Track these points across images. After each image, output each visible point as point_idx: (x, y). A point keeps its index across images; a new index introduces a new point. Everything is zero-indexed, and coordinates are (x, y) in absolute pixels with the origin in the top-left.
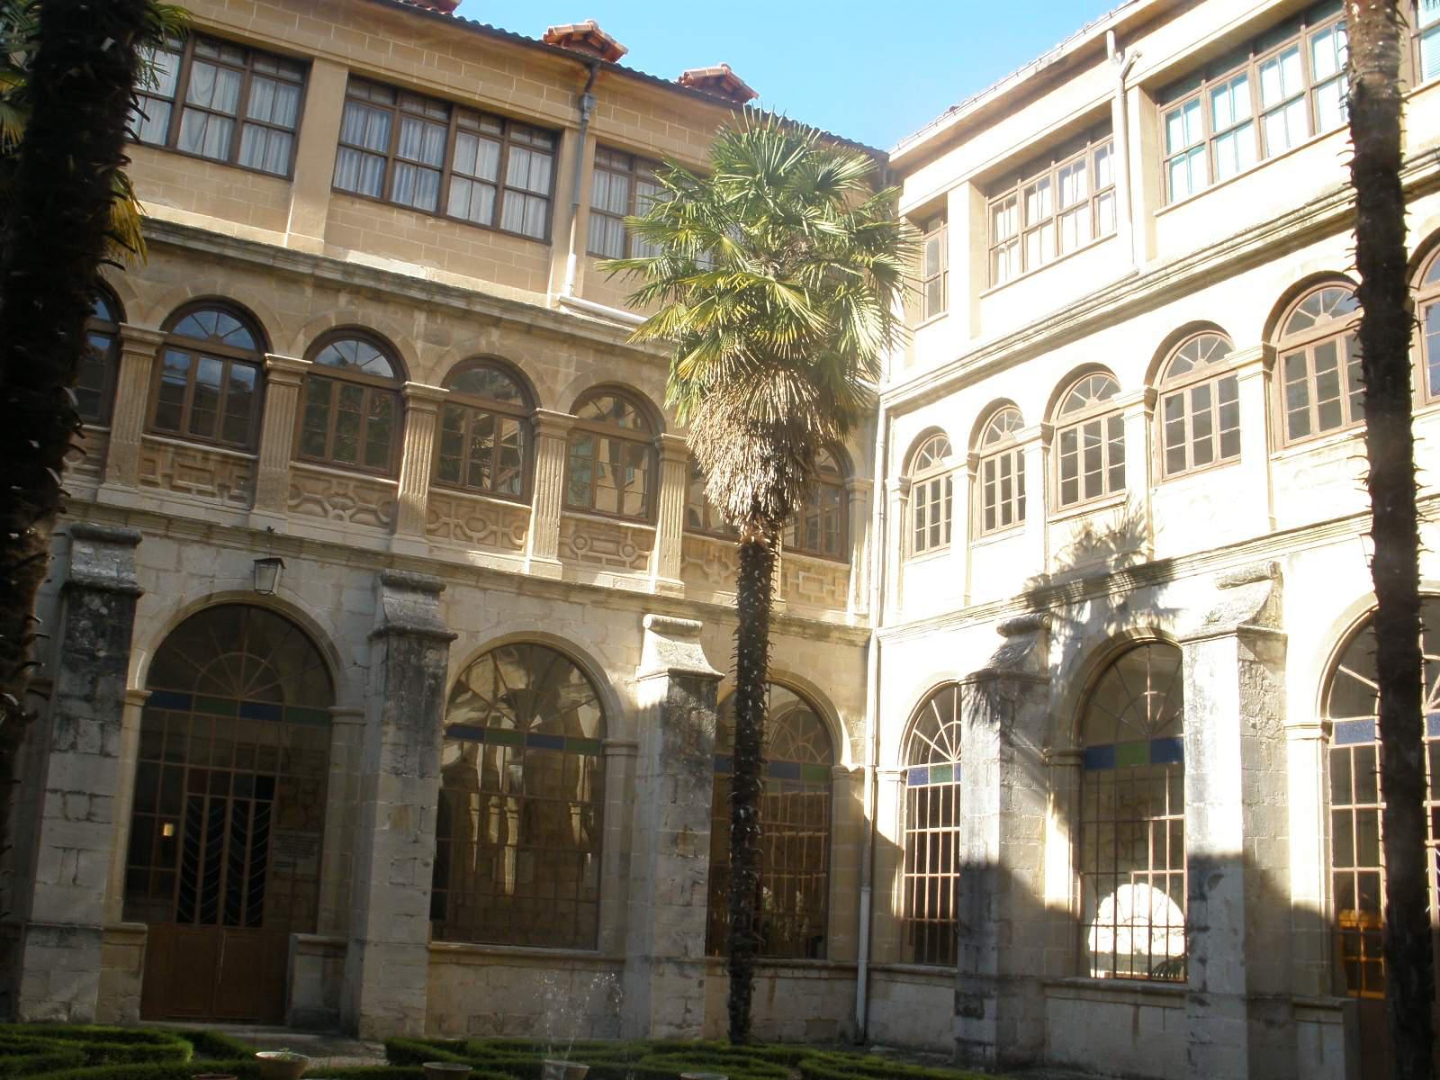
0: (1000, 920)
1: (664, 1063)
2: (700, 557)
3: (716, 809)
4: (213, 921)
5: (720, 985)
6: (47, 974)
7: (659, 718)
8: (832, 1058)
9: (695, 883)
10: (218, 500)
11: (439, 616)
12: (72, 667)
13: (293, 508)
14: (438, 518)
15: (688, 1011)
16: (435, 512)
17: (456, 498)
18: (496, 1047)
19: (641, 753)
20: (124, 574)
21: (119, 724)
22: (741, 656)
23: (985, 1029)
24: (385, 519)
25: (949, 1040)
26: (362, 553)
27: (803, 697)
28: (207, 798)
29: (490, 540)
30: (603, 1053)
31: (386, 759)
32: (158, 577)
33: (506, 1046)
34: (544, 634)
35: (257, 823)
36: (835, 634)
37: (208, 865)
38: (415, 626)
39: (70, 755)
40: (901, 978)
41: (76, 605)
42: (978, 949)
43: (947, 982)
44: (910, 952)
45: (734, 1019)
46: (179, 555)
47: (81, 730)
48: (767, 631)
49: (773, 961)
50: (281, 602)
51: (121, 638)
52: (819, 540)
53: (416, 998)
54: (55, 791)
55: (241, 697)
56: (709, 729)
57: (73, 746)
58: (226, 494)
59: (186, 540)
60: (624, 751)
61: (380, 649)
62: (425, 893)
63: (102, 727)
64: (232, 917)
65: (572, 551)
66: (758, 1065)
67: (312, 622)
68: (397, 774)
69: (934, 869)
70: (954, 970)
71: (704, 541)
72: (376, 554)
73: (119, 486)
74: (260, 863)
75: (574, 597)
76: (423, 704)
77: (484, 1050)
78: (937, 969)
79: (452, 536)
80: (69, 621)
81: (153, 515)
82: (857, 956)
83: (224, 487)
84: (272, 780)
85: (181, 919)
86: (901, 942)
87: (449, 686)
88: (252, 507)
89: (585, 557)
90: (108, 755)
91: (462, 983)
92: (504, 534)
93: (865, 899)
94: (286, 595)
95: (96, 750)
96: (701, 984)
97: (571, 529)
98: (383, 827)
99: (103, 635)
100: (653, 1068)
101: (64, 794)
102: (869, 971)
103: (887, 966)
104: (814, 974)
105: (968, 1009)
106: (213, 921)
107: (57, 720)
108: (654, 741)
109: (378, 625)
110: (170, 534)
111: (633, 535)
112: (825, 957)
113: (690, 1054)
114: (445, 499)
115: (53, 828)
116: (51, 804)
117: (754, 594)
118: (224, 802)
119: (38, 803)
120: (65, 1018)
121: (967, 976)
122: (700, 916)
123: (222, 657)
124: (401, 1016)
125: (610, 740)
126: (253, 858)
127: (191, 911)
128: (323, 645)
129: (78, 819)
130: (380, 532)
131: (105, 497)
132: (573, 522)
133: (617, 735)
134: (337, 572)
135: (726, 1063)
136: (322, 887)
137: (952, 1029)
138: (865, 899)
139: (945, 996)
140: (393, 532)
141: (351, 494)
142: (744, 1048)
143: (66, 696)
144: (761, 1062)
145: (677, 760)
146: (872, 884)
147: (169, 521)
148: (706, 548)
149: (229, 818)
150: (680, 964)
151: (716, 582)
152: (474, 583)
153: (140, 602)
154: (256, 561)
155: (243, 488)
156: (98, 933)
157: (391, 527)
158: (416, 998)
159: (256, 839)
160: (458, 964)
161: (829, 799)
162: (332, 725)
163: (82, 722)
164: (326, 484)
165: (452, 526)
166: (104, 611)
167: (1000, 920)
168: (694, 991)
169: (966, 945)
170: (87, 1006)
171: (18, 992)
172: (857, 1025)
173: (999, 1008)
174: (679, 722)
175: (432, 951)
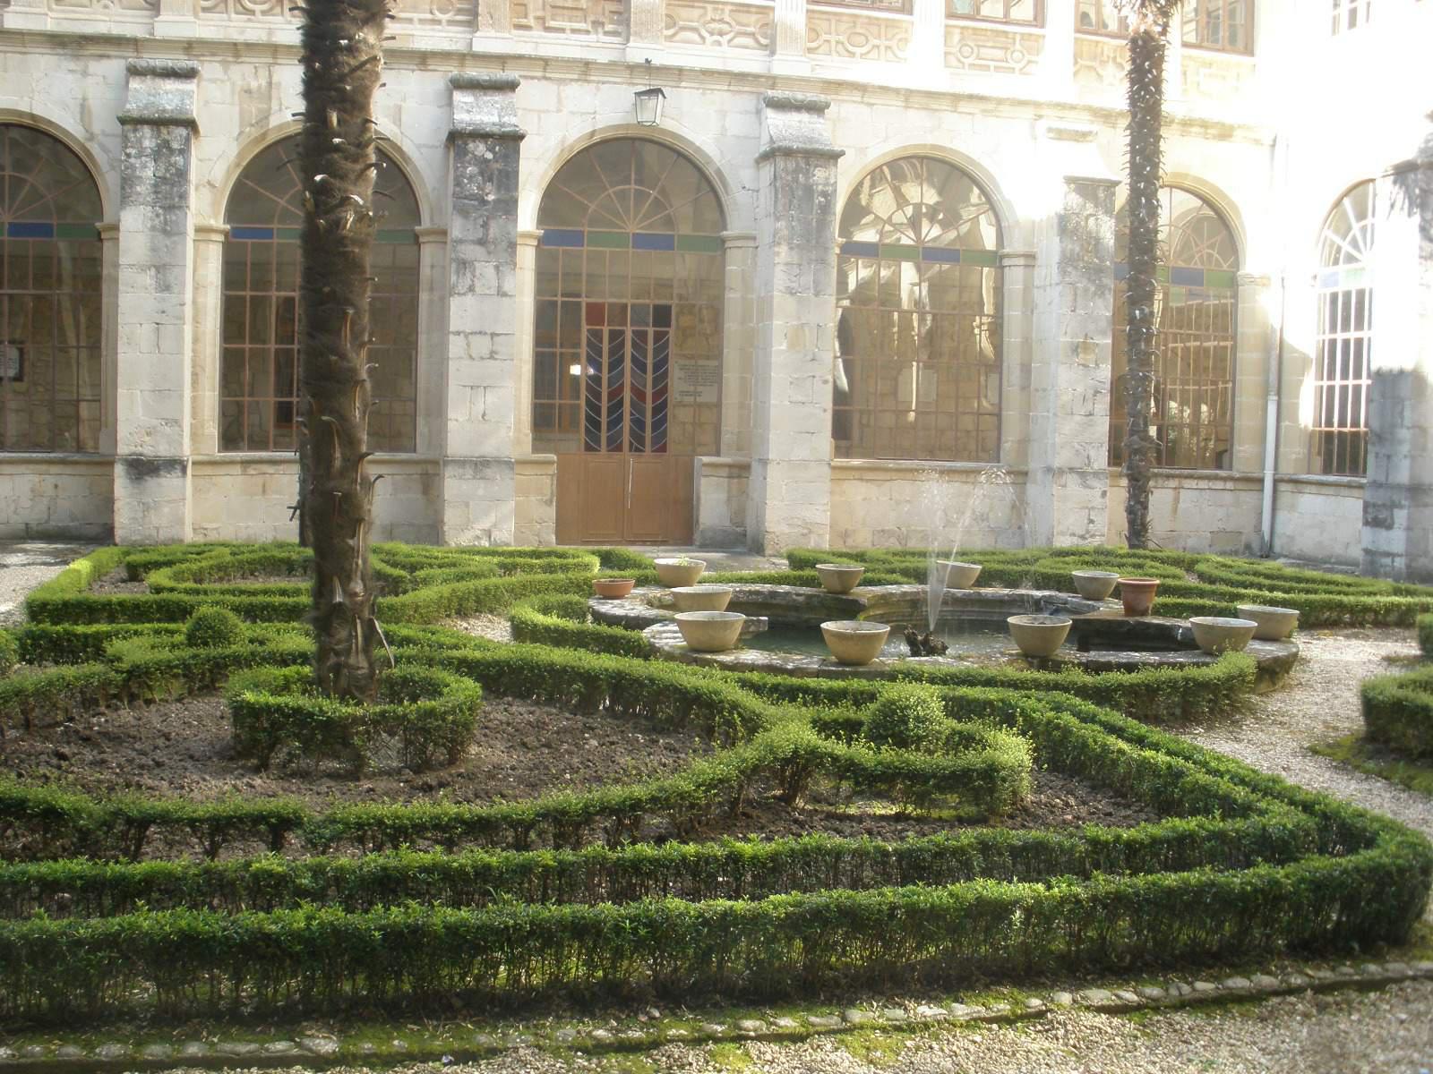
0: (1414, 427)
1: (1061, 565)
2: (1095, 58)
3: (1115, 318)
4: (619, 448)
5: (1119, 494)
6: (467, 505)
7: (1055, 226)
8: (1230, 563)
9: (1097, 392)
10: (593, 37)
11: (825, 134)
12: (464, 213)
13: (670, 38)
14: (818, 35)
15: (1091, 521)
16: (814, 30)
17: (835, 14)
18: (895, 554)
19: (1039, 262)
20: (505, 119)
21: (513, 264)
22: (1133, 152)
23: (1395, 540)
24: (764, 41)
25: (1356, 553)
26: (741, 77)
27: (1206, 201)
28: (606, 330)
29: (874, 54)
30: (1002, 558)
31: (780, 279)
32: (539, 118)
33: (904, 554)
34: (934, 147)
35: (657, 351)
36: (1237, 133)
37: (611, 395)
38: (801, 145)
39: (469, 298)
40: (1308, 489)
41: (461, 153)
42: (1389, 457)
43: (1356, 492)
44: (1318, 462)
45: (1132, 523)
46: (559, 94)
47: (477, 273)
48: (1160, 125)
49: (1178, 472)
50: (664, 131)
51: (507, 179)
52: (1221, 34)
53: (820, 514)
54: (458, 333)
55: (633, 228)
56: (1108, 237)
57: (471, 289)
58: (600, 30)
59: (564, 80)
60: (1022, 261)
61: (767, 171)
62: (825, 411)
63: (497, 268)
64: (638, 445)
65: (959, 61)
66: (1152, 567)
67: (698, 149)
68: (791, 294)
69: (1345, 376)
70: (1364, 481)
71: (1097, 42)
72: (757, 77)
73: (492, 33)
74: (661, 392)
75: (964, 107)
76: (814, 224)
77: (883, 557)
78: (1346, 479)
79: (834, 53)
80: (456, 169)
81: (530, 58)
82: (1262, 466)
83: (597, 24)
84: (669, 308)
85: (589, 448)
86: (1310, 452)
87: (839, 205)
88: (628, 40)
89: (972, 66)
90: (505, 295)
91: (864, 499)
92: (888, 48)
93: (1272, 408)
94: (668, 124)
95: (493, 291)
96: (1104, 494)
97: (956, 38)
98: (779, 346)
99: (490, 180)
100: (1050, 571)
101: (467, 335)
102: (1276, 482)
103: (1294, 477)
104: (1220, 485)
105: (1376, 519)
106: (619, 448)
107: (454, 265)
108: (1051, 249)
109: (765, 148)
110: (548, 75)
111: (1022, 39)
112: (1231, 468)
113: (1087, 558)
114: (825, 16)
115: (459, 371)
116: (455, 346)
117: (1144, 87)
118: (622, 333)
119: (442, 347)
120: (487, 544)
121: (1376, 485)
122: (1102, 426)
123: (611, 191)
124: (805, 531)
125: (1007, 250)
126: (654, 386)
127: (598, 442)
128: (710, 171)
129: (482, 358)
130: (760, 54)
131: (479, 47)
132: (957, 31)
133: (1014, 245)
134: (720, 97)
135: (1120, 566)
136: (724, 411)
137: (1360, 542)
138: (1272, 408)
139: (1351, 507)
140: (773, 53)
141: (727, 19)
142: (1141, 552)
143: (461, 241)
144: (1158, 564)
145: (1076, 268)
146: (1279, 393)
147: (546, 62)
148: (1099, 50)
149: (628, 349)
150: (1083, 475)
151: (1111, 85)
152: (859, 99)
153: (523, 145)
154: (638, 94)
155: (619, 23)
156: (509, 464)
157: (771, 49)
158: (820, 514)
159: (657, 367)
160: (862, 480)
161: (1235, 305)
162: (724, 251)
163: (477, 264)
164: (701, 11)
165: (833, 43)
166: (489, 156)
167: (1414, 427)
168: (1098, 501)
169: (1377, 454)
170: (507, 536)
171: (442, 521)
172: (1263, 538)
173: (1409, 518)
174: (1076, 230)
175: (834, 468)
